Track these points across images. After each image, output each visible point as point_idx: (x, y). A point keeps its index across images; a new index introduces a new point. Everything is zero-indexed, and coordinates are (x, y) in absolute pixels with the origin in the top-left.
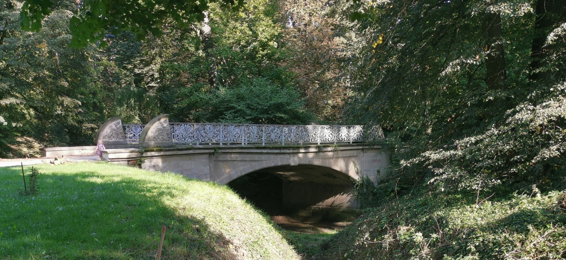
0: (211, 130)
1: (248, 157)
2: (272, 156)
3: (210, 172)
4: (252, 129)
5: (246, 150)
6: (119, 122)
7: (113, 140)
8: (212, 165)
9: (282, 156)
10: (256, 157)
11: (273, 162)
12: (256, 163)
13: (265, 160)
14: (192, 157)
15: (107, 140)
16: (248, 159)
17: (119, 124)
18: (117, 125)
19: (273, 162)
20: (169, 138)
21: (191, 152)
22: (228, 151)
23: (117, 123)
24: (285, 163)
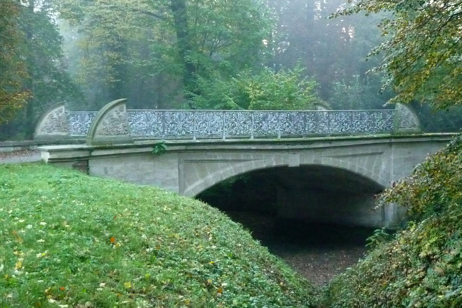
0: (182, 120)
1: (230, 156)
2: (264, 155)
3: (179, 177)
4: (236, 117)
5: (147, 149)
6: (62, 109)
7: (55, 133)
8: (181, 166)
9: (278, 154)
10: (242, 156)
11: (265, 162)
12: (242, 164)
13: (255, 160)
14: (64, 163)
15: (46, 133)
16: (230, 159)
17: (61, 112)
18: (59, 112)
19: (265, 162)
20: (126, 130)
21: (407, 140)
22: (207, 147)
23: (59, 111)
24: (395, 139)
